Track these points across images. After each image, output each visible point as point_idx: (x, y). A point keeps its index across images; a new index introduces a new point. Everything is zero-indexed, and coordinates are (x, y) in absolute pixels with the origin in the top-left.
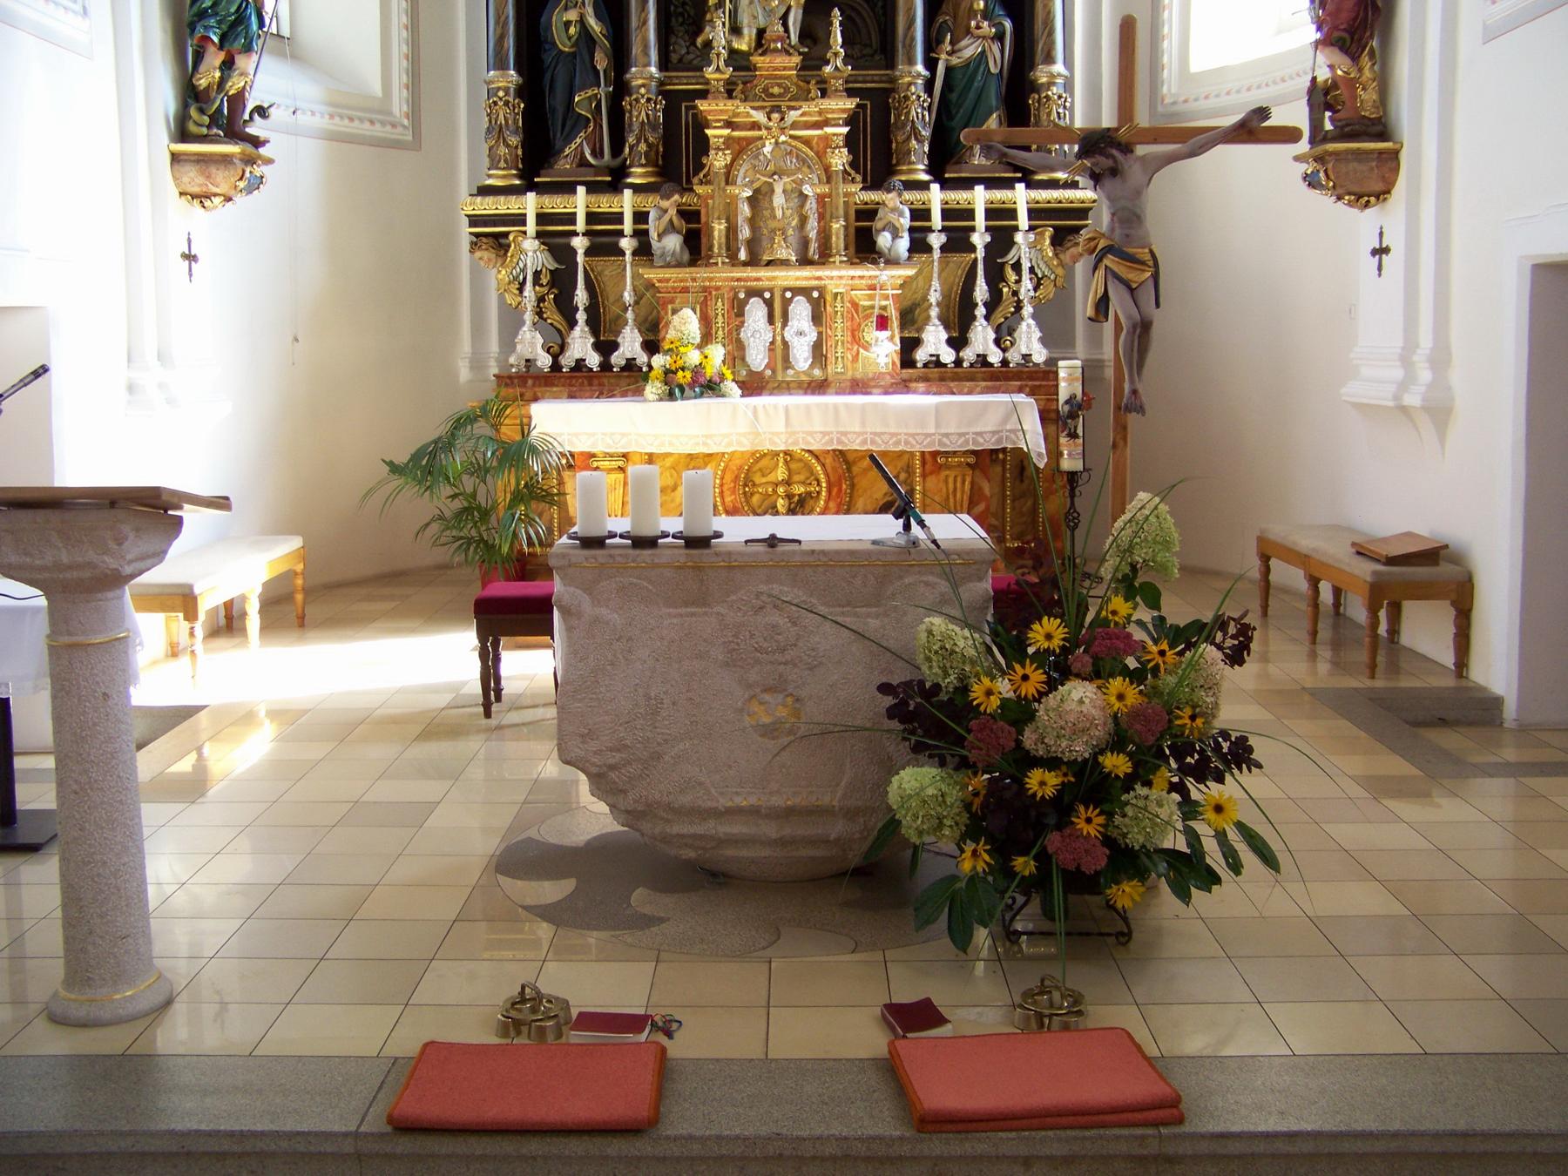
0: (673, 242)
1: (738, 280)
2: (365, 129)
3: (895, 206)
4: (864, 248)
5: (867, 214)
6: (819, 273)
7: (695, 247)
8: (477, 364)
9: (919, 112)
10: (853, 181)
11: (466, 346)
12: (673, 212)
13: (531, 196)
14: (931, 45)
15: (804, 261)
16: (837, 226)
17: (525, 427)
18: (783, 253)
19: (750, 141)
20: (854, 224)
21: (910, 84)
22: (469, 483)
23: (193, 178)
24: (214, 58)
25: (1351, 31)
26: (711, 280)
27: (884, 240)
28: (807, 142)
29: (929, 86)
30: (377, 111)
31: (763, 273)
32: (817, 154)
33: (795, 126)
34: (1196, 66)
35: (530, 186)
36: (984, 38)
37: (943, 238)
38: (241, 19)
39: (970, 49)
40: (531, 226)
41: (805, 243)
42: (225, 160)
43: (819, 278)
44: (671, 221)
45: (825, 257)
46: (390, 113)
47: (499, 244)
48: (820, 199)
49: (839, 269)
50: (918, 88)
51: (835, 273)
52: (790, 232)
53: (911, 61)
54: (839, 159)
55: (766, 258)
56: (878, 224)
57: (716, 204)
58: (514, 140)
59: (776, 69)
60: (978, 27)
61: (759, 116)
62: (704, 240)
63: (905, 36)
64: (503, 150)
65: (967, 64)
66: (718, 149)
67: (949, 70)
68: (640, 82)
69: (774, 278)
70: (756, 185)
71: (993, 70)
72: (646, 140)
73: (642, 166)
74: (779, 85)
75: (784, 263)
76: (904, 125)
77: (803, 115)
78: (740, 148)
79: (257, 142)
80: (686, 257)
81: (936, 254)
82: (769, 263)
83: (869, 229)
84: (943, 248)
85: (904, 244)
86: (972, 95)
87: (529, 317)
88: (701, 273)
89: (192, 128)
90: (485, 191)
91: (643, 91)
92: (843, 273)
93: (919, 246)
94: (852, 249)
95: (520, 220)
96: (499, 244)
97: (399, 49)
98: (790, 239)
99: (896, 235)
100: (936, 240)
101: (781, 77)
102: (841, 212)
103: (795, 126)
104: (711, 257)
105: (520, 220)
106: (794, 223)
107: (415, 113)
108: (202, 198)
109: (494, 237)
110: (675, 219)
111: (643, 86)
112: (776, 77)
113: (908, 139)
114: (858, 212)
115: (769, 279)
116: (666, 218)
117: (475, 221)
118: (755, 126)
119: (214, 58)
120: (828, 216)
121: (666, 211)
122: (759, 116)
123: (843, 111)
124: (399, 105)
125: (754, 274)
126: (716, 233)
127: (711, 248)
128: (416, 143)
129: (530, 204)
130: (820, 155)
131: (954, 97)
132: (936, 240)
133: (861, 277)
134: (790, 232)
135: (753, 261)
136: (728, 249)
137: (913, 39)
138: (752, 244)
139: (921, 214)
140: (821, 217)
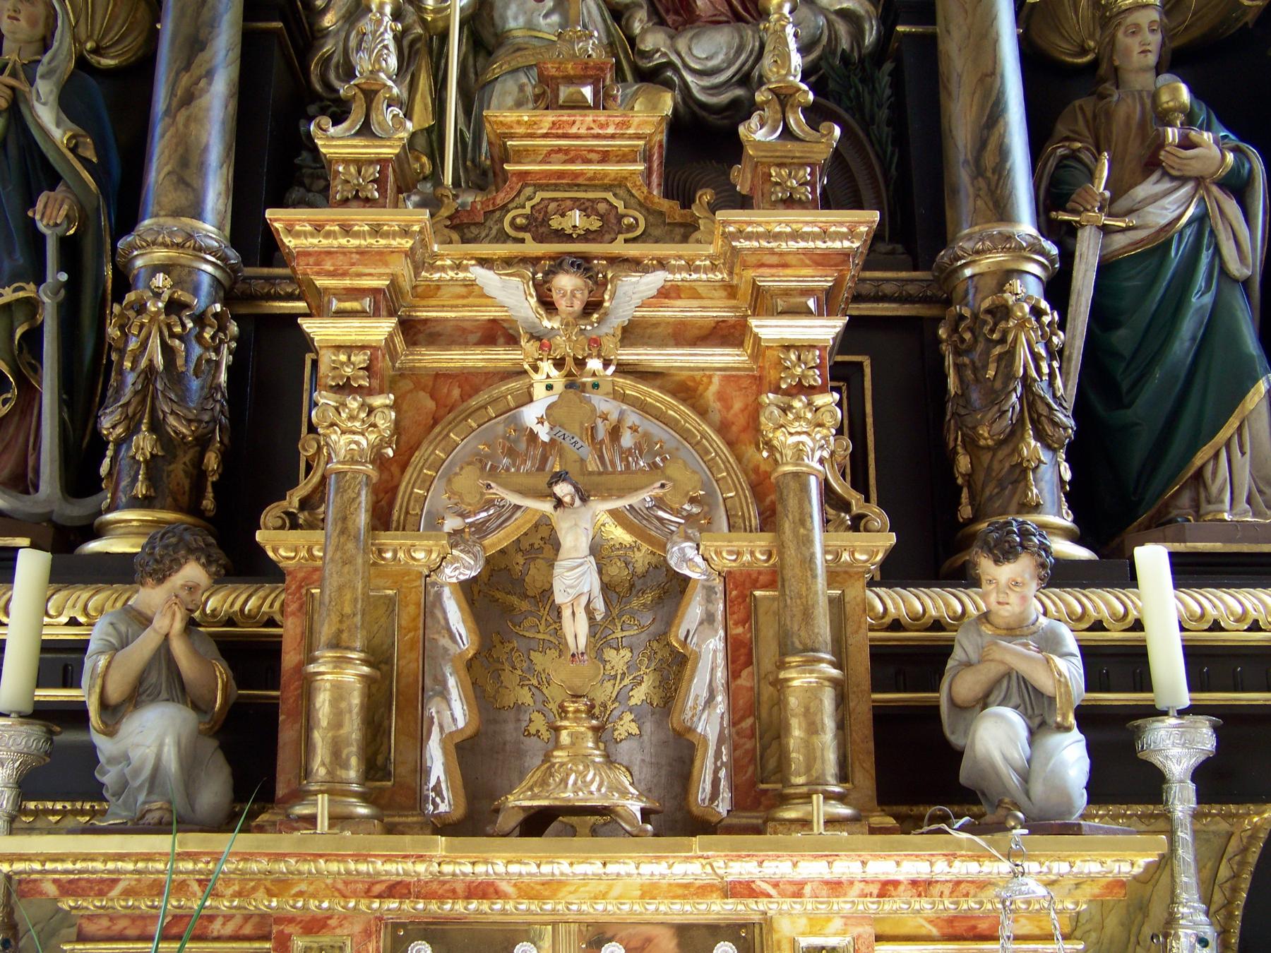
0: (153, 737)
1: (396, 889)
3: (1019, 613)
4: (916, 769)
5: (913, 662)
6: (743, 869)
7: (250, 758)
9: (1045, 358)
10: (858, 524)
12: (168, 623)
14: (1054, 198)
15: (677, 819)
16: (809, 683)
18: (585, 785)
19: (471, 381)
20: (866, 700)
21: (1008, 274)
25: (803, 826)
26: (279, 885)
27: (997, 738)
28: (686, 390)
29: (1058, 288)
31: (508, 863)
32: (723, 429)
33: (632, 333)
36: (1199, 181)
37: (1204, 738)
39: (1166, 207)
41: (679, 755)
43: (744, 890)
44: (164, 651)
45: (760, 801)
48: (739, 589)
49: (828, 852)
50: (1029, 287)
51: (812, 869)
52: (626, 725)
53: (1002, 210)
54: (808, 439)
55: (520, 799)
56: (961, 683)
57: (341, 593)
59: (572, 156)
60: (1187, 144)
61: (510, 295)
62: (287, 734)
63: (982, 145)
65: (1158, 248)
66: (345, 388)
67: (1106, 269)
68: (160, 255)
69: (552, 886)
70: (498, 540)
71: (1234, 267)
72: (157, 426)
73: (135, 503)
74: (588, 208)
75: (597, 821)
76: (996, 397)
77: (665, 293)
78: (434, 408)
80: (214, 790)
81: (1182, 800)
82: (537, 823)
83: (932, 712)
84: (1214, 780)
85: (1071, 756)
86: (1188, 327)
88: (239, 852)
91: (160, 280)
92: (846, 867)
93: (1123, 777)
94: (865, 779)
98: (625, 751)
99: (1039, 713)
100: (1179, 747)
101: (593, 183)
102: (823, 627)
103: (632, 333)
104: (300, 795)
106: (639, 695)
110: (179, 648)
111: (166, 268)
112: (574, 182)
113: (1014, 434)
114: (880, 655)
115: (527, 892)
116: (146, 644)
118: (498, 333)
120: (767, 653)
121: (144, 621)
122: (510, 295)
123: (822, 260)
125: (394, 869)
126: (323, 703)
127: (306, 772)
130: (744, 432)
131: (1123, 338)
132: (1179, 747)
133: (921, 886)
134: (626, 725)
135: (475, 822)
136: (374, 767)
137: (1003, 153)
138: (480, 757)
139: (1117, 663)
140: (740, 655)
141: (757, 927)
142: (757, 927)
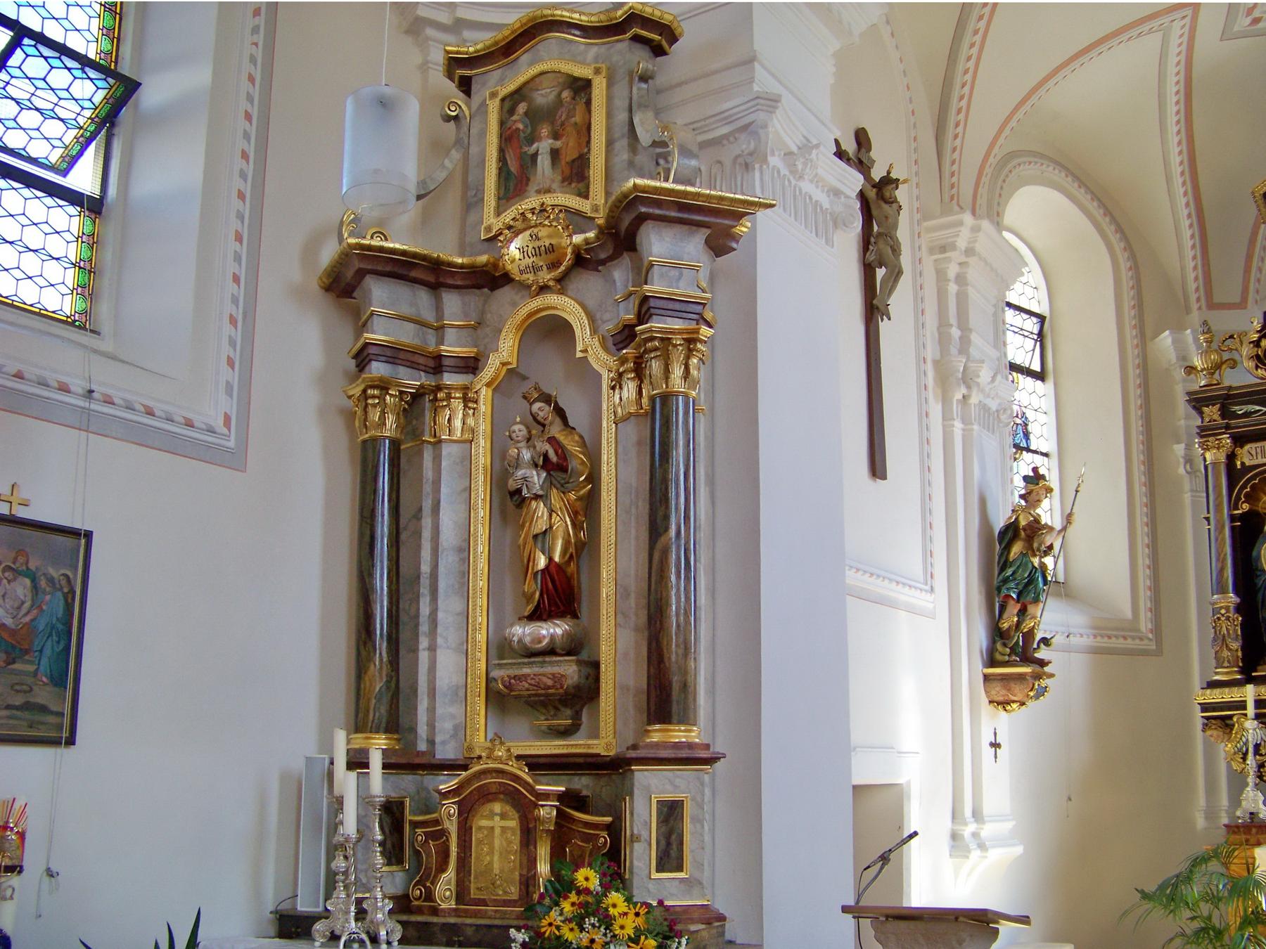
2: (1119, 643)
8: (1211, 814)
11: (1201, 801)
13: (1250, 688)
17: (1250, 866)
22: (1205, 908)
23: (999, 692)
24: (1013, 609)
30: (1129, 629)
34: (636, 774)
35: (1249, 680)
38: (1031, 581)
40: (1251, 710)
42: (1021, 677)
46: (1139, 630)
47: (1226, 724)
58: (1236, 645)
64: (1226, 653)
79: (1042, 663)
87: (1251, 780)
89: (998, 657)
90: (1212, 685)
95: (1242, 705)
96: (1226, 724)
97: (1144, 581)
105: (1242, 705)
107: (1157, 629)
108: (1004, 704)
109: (1221, 719)
117: (1205, 707)
119: (1013, 609)
124: (1145, 625)
128: (1159, 652)
129: (1249, 693)
141: (1250, 455)
142: (1250, 455)
